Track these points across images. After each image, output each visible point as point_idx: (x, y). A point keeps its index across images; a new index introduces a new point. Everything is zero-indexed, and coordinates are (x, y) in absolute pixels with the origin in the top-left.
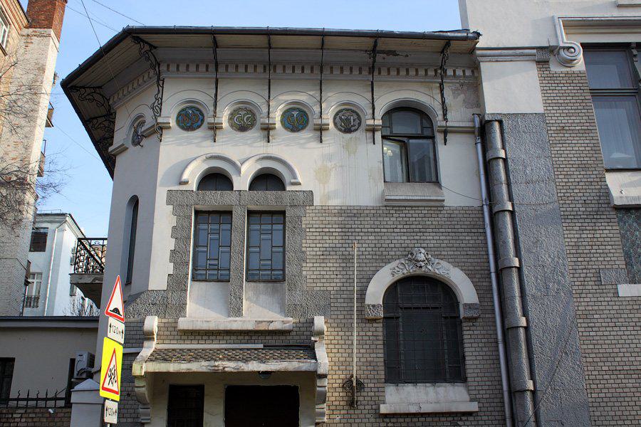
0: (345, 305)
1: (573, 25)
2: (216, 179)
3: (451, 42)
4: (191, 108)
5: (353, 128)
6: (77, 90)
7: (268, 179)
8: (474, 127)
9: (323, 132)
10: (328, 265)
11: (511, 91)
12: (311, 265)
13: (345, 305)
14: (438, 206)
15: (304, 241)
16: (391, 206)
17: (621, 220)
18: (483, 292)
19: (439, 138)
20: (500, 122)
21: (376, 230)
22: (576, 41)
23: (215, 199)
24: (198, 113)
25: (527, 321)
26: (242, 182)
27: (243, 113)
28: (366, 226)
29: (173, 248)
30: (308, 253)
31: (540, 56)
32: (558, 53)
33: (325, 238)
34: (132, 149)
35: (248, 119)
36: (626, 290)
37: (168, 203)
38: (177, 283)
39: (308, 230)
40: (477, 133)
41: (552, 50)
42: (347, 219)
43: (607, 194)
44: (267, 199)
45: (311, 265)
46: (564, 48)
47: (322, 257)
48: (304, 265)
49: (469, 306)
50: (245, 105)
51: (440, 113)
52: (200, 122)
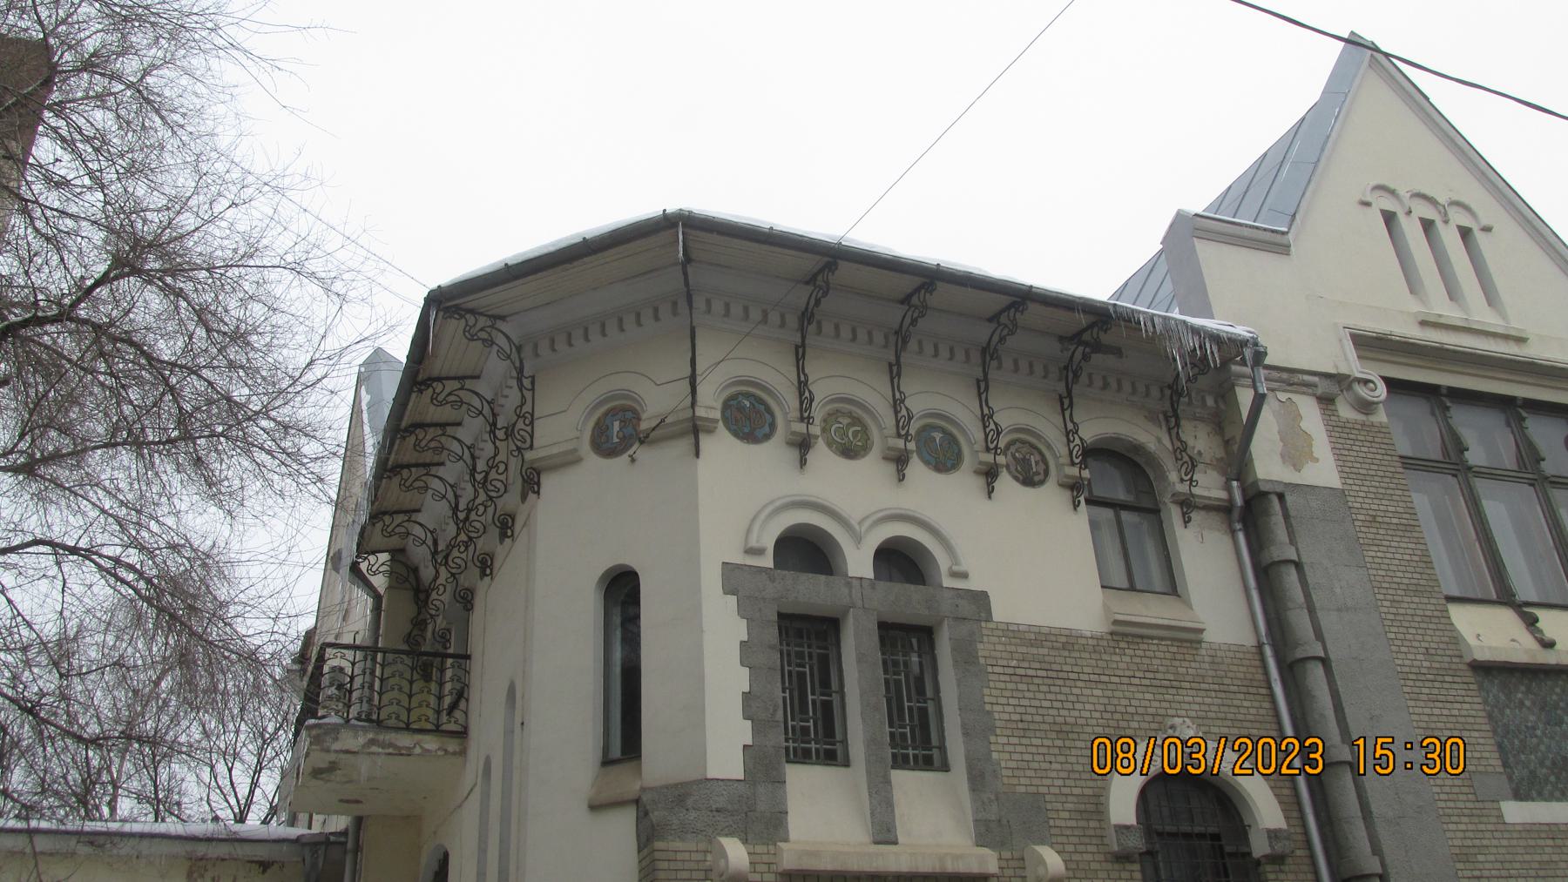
0: (1073, 824)
1: (1370, 345)
2: (806, 550)
3: (939, 284)
4: (748, 395)
5: (1036, 478)
6: (462, 317)
7: (901, 560)
8: (1231, 500)
9: (702, 437)
10: (1035, 741)
11: (1297, 451)
12: (1005, 740)
13: (1073, 824)
14: (1188, 639)
15: (986, 691)
16: (1124, 634)
17: (1481, 688)
18: (1291, 805)
19: (1174, 513)
20: (1281, 497)
21: (1104, 678)
22: (1373, 372)
23: (810, 592)
24: (762, 408)
25: (1383, 864)
26: (859, 562)
27: (846, 421)
28: (1086, 670)
29: (747, 689)
30: (996, 716)
31: (1324, 387)
32: (1349, 388)
33: (1021, 686)
34: (593, 461)
35: (855, 434)
36: (1515, 812)
37: (728, 590)
38: (763, 766)
39: (990, 669)
40: (1236, 514)
41: (1341, 381)
42: (1053, 653)
43: (1455, 639)
44: (905, 601)
45: (1005, 740)
46: (1359, 381)
47: (1020, 725)
48: (993, 739)
49: (1273, 835)
50: (853, 408)
51: (793, 402)
52: (767, 429)
